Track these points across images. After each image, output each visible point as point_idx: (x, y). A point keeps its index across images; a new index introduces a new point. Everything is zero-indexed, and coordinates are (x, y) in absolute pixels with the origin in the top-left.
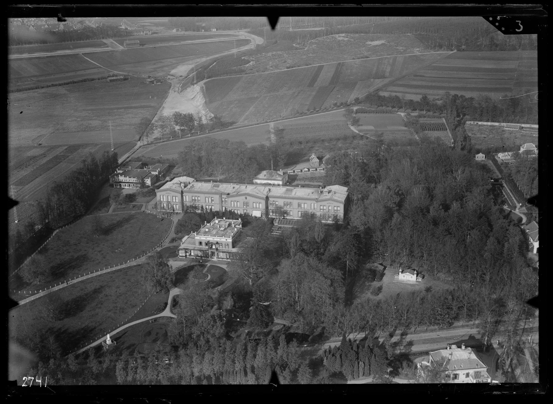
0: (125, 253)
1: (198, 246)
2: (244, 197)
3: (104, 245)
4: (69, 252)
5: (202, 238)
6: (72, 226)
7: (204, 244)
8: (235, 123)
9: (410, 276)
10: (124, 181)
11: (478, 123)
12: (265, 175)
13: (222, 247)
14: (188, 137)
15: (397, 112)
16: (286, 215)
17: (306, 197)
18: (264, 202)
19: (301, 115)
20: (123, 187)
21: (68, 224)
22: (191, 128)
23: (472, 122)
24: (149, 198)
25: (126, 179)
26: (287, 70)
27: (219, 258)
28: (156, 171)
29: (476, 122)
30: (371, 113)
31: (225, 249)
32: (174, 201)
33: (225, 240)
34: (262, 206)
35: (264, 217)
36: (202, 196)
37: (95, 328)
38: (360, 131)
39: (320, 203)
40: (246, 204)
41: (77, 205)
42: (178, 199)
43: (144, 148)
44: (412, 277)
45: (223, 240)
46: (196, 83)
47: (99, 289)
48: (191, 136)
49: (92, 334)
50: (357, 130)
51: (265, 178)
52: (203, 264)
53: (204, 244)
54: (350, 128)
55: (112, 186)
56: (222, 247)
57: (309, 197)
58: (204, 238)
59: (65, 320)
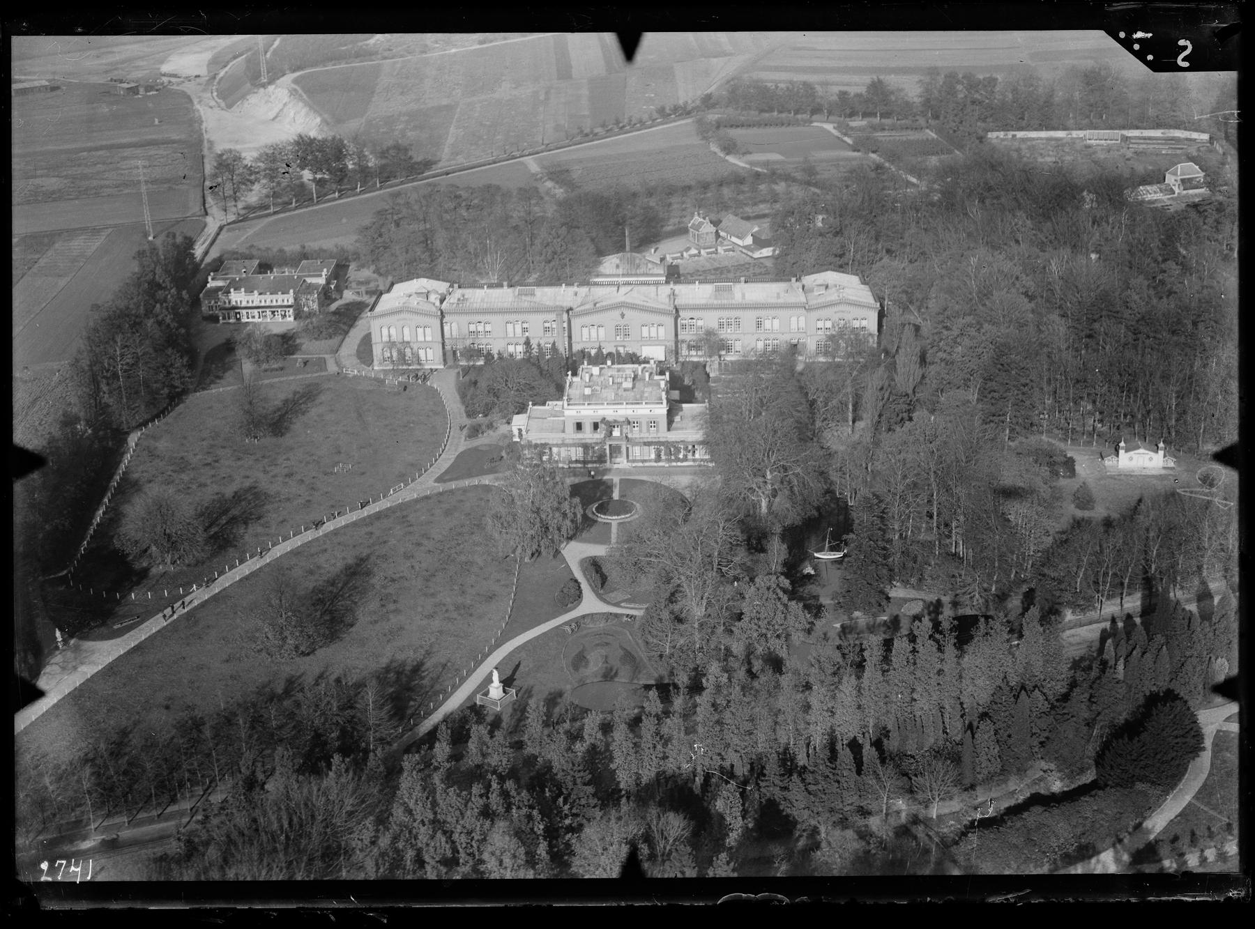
0: (363, 474)
1: (571, 435)
2: (617, 313)
3: (288, 459)
4: (203, 485)
5: (584, 413)
6: (170, 418)
7: (588, 427)
8: (435, 163)
9: (1147, 457)
10: (244, 304)
11: (1014, 136)
12: (618, 266)
13: (641, 431)
14: (335, 199)
15: (811, 122)
16: (723, 353)
17: (774, 301)
18: (669, 321)
19: (587, 139)
20: (244, 320)
21: (158, 416)
22: (341, 176)
23: (1001, 134)
24: (336, 340)
25: (250, 298)
26: (478, 47)
27: (634, 461)
28: (321, 276)
29: (1010, 134)
30: (754, 126)
31: (647, 435)
32: (421, 338)
33: (646, 412)
34: (664, 332)
35: (673, 360)
36: (497, 319)
37: (421, 664)
38: (751, 163)
39: (815, 314)
40: (620, 330)
41: (172, 365)
42: (429, 334)
43: (234, 229)
44: (1151, 459)
45: (643, 411)
46: (270, 83)
47: (358, 565)
48: (340, 198)
49: (422, 678)
50: (746, 163)
51: (620, 271)
52: (596, 478)
53: (588, 427)
54: (780, 153)
55: (214, 319)
56: (641, 431)
57: (781, 301)
58: (591, 413)
59: (320, 653)
